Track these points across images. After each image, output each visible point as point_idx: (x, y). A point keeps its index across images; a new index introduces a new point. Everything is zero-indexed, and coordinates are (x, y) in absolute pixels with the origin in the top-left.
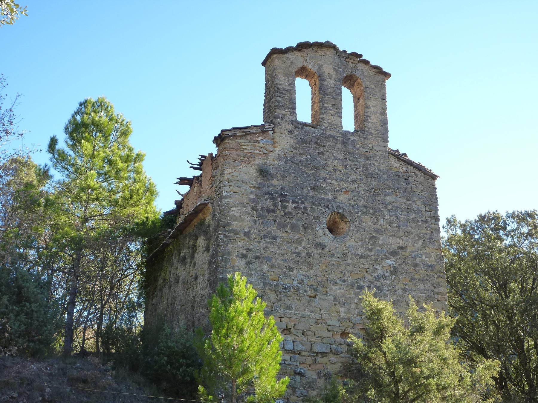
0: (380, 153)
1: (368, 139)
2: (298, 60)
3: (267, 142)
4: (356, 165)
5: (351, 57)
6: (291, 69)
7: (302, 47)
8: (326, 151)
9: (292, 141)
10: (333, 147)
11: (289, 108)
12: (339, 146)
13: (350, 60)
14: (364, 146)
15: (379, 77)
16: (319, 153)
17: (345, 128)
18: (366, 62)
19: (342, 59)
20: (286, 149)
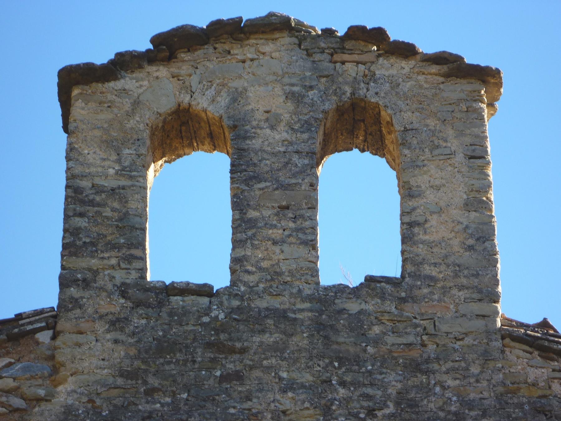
0: (468, 341)
1: (415, 300)
2: (159, 91)
3: (25, 369)
4: (368, 397)
5: (348, 45)
6: (131, 123)
7: (172, 45)
8: (251, 368)
9: (121, 351)
10: (278, 349)
11: (114, 247)
12: (301, 340)
13: (346, 57)
14: (401, 326)
15: (458, 89)
16: (223, 378)
17: (161, 267)
18: (406, 50)
19: (317, 57)
20: (97, 382)
